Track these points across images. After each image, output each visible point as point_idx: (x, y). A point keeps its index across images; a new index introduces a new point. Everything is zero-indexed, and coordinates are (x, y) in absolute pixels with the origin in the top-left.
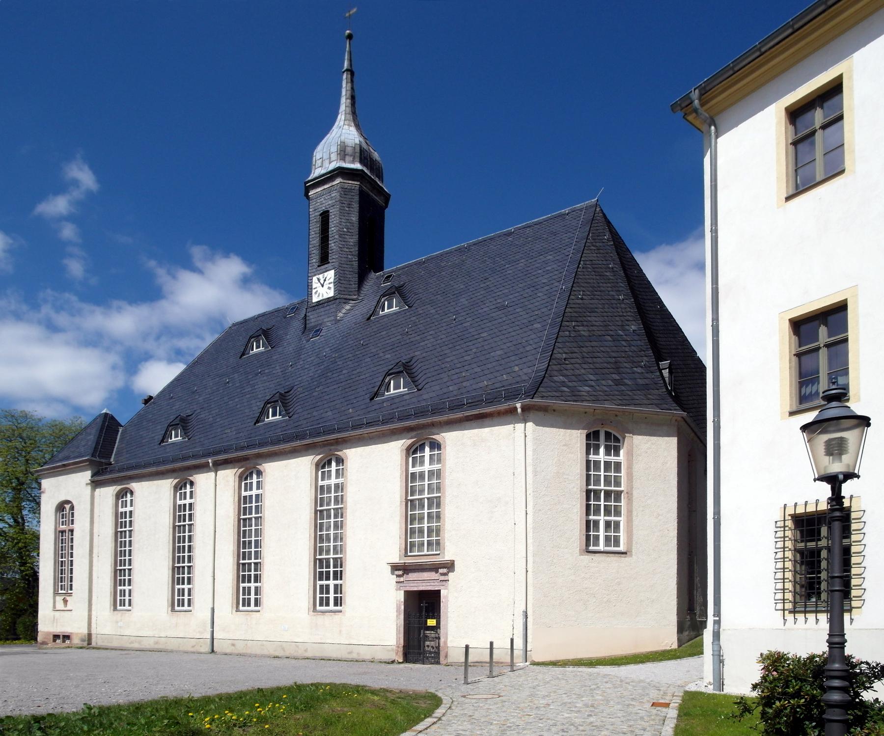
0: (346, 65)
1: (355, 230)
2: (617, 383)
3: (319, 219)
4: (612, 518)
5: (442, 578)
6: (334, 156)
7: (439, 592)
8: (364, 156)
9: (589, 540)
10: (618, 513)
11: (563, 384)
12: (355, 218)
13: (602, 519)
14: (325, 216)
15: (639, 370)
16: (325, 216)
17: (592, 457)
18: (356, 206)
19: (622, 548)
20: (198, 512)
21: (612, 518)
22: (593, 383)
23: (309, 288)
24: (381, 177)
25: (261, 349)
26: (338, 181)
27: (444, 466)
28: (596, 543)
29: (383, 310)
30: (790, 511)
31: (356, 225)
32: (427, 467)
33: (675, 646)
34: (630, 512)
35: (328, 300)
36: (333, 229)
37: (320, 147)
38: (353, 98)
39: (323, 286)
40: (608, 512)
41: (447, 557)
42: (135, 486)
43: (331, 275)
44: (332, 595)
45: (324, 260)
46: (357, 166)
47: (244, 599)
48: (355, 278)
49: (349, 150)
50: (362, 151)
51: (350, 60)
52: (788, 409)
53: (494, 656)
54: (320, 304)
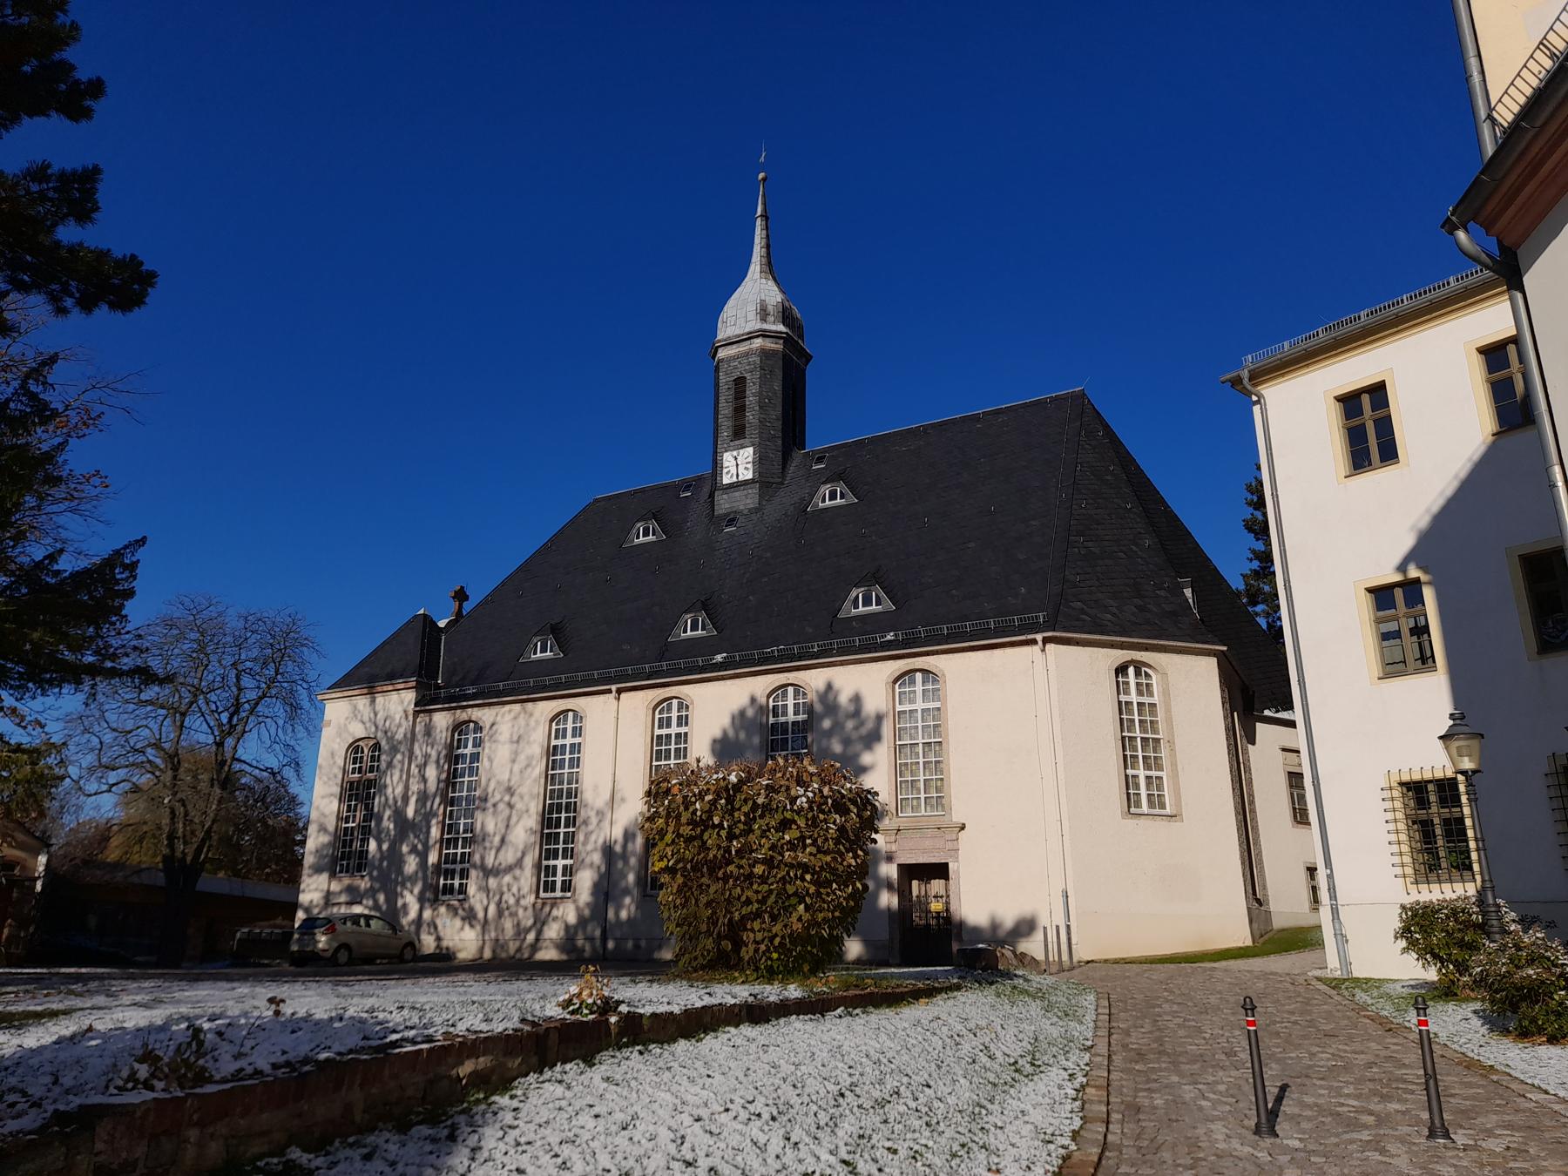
0: (759, 212)
1: (778, 401)
2: (1142, 609)
3: (732, 385)
4: (1153, 773)
5: (950, 845)
6: (752, 315)
7: (946, 865)
8: (786, 316)
9: (1131, 800)
10: (1160, 768)
11: (1082, 611)
12: (777, 386)
13: (1142, 773)
14: (740, 382)
15: (1162, 593)
16: (740, 382)
17: (1123, 698)
18: (779, 374)
19: (1168, 811)
20: (587, 756)
21: (1153, 773)
22: (1115, 610)
23: (716, 466)
24: (801, 337)
25: (651, 538)
26: (758, 343)
27: (945, 703)
28: (1138, 805)
29: (824, 501)
30: (1395, 779)
31: (780, 394)
32: (919, 705)
33: (1249, 943)
34: (1174, 765)
35: (746, 483)
36: (751, 399)
37: (731, 302)
38: (768, 246)
39: (738, 464)
40: (1148, 767)
41: (957, 818)
42: (484, 715)
43: (748, 453)
44: (559, 878)
45: (739, 433)
46: (781, 328)
47: (546, 882)
48: (777, 457)
49: (770, 309)
50: (785, 309)
51: (764, 204)
52: (1376, 675)
53: (1274, 906)
54: (731, 486)
